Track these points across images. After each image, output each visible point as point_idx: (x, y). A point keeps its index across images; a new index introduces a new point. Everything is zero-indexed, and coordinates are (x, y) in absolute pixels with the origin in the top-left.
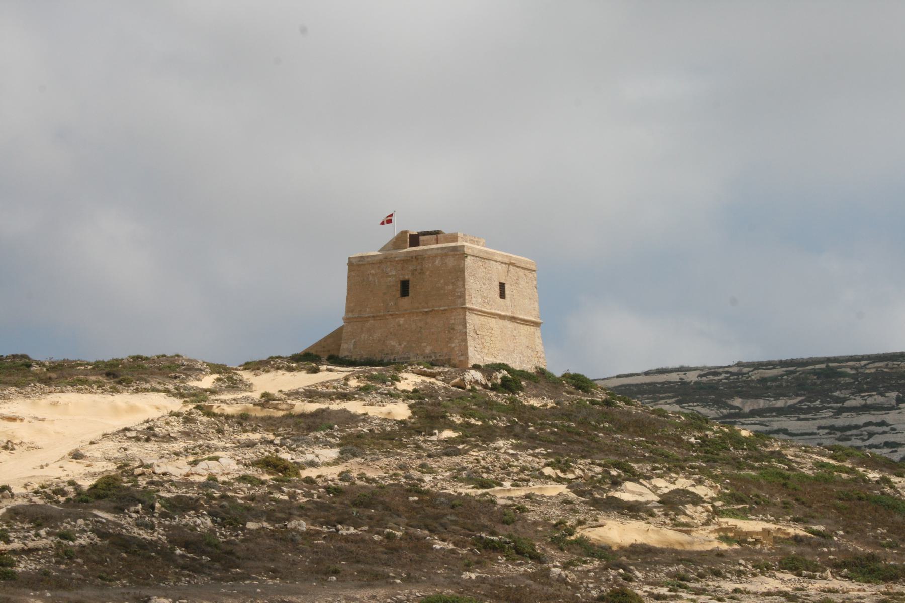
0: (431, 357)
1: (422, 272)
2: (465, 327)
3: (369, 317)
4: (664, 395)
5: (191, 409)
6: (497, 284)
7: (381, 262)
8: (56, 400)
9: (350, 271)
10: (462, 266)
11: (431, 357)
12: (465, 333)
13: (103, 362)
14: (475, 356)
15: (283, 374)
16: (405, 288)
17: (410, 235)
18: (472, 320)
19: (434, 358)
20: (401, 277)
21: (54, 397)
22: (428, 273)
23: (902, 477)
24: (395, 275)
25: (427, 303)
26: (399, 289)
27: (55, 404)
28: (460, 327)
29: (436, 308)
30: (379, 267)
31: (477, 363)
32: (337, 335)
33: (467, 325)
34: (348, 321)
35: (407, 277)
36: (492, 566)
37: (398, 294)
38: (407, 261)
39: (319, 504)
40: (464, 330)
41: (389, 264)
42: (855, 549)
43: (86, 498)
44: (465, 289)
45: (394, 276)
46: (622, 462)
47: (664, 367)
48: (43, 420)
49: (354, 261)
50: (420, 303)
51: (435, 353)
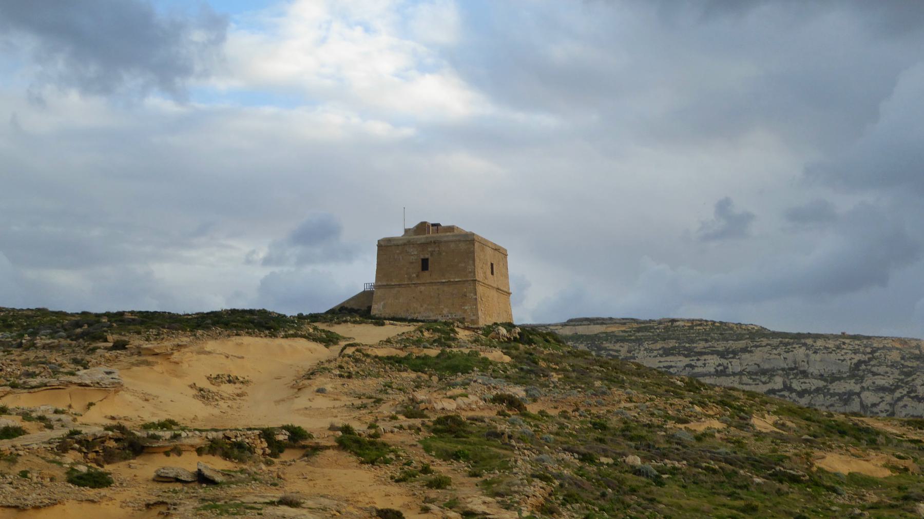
0: (448, 316)
1: (440, 253)
3: (395, 285)
5: (354, 352)
6: (489, 264)
7: (405, 244)
8: (240, 341)
9: (379, 250)
10: (472, 249)
11: (448, 316)
13: (832, 335)
16: (425, 265)
18: (480, 289)
20: (422, 257)
21: (236, 340)
22: (444, 254)
23: (922, 429)
27: (238, 344)
29: (452, 280)
32: (367, 296)
35: (427, 256)
36: (901, 464)
37: (420, 268)
40: (475, 297)
41: (412, 246)
43: (510, 413)
45: (415, 255)
47: (64, 311)
48: (243, 358)
49: (382, 243)
51: (451, 314)
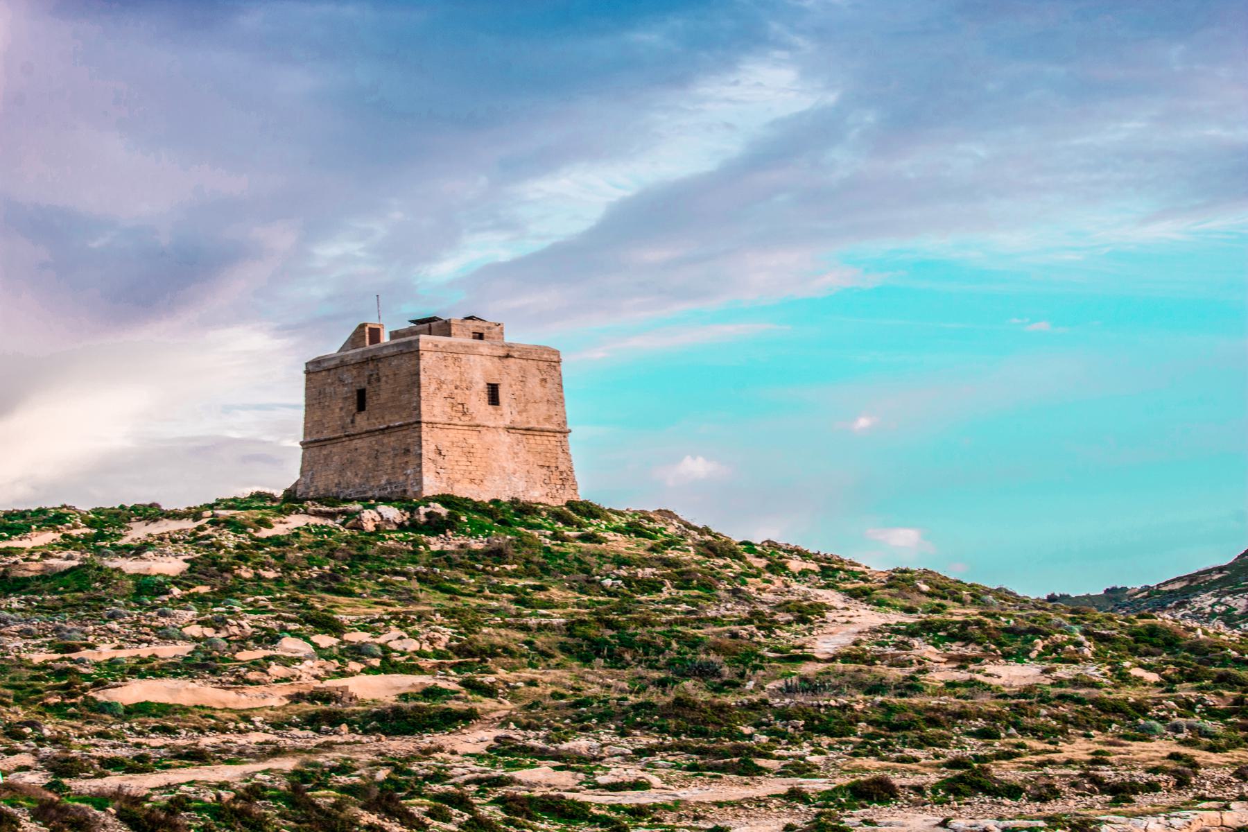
2: (420, 447)
4: (328, 509)
12: (421, 455)
14: (431, 485)
15: (167, 524)
17: (370, 329)
19: (389, 490)
23: (8, 787)
24: (352, 383)
25: (383, 418)
26: (356, 402)
28: (416, 448)
30: (335, 374)
31: (495, 497)
33: (424, 443)
34: (305, 446)
37: (354, 408)
38: (363, 362)
39: (397, 670)
40: (419, 452)
42: (749, 700)
44: (420, 397)
46: (154, 666)
50: (377, 419)
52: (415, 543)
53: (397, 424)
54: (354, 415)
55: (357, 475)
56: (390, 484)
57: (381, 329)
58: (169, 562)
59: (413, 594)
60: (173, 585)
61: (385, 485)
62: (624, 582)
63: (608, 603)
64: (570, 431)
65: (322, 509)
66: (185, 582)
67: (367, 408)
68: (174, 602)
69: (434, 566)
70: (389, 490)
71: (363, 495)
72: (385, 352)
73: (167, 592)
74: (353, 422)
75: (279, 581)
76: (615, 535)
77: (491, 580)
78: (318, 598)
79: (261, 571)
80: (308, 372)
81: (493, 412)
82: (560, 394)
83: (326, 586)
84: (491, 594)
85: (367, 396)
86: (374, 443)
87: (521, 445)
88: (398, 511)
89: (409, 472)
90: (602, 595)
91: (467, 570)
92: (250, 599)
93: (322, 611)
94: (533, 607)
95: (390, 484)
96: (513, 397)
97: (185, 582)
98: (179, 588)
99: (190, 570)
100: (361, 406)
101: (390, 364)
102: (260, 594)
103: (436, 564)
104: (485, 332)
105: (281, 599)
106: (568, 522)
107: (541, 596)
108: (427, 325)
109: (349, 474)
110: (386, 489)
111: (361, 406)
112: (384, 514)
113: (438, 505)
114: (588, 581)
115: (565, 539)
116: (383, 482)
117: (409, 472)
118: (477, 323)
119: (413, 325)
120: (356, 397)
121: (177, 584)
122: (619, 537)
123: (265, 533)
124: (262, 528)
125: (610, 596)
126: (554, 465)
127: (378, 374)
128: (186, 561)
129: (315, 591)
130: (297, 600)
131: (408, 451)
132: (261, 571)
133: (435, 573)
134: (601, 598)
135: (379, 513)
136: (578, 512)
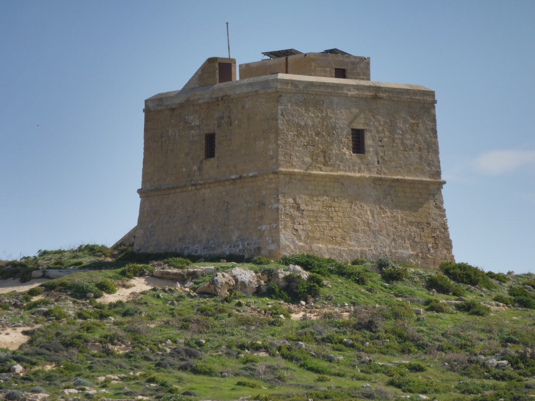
24: (199, 126)
26: (204, 147)
37: (202, 154)
40: (275, 206)
52: (275, 313)
53: (251, 174)
54: (202, 162)
55: (204, 229)
56: (243, 240)
57: (233, 64)
58: (7, 334)
59: (278, 374)
60: (15, 362)
61: (237, 241)
62: (510, 361)
63: (494, 388)
64: (444, 183)
65: (170, 270)
66: (28, 358)
67: (216, 154)
68: (19, 381)
69: (299, 340)
70: (241, 247)
71: (340, 353)
72: (238, 91)
73: (10, 370)
74: (200, 169)
75: (130, 357)
76: (498, 305)
77: (361, 357)
78: (176, 377)
79: (110, 346)
80: (147, 111)
81: (359, 161)
82: (433, 139)
83: (183, 363)
84: (363, 374)
85: (216, 141)
86: (224, 194)
87: (389, 198)
88: (254, 274)
89: (264, 228)
90: (487, 378)
91: (334, 345)
92: (102, 379)
93: (184, 394)
94: (410, 391)
95: (243, 240)
96: (380, 144)
97: (28, 358)
98: (22, 365)
99: (30, 342)
100: (210, 152)
101: (243, 107)
102: (112, 373)
103: (300, 338)
104: (348, 68)
105: (135, 378)
106: (443, 290)
107: (419, 377)
108: (284, 59)
109: (195, 227)
110: (238, 246)
111: (210, 152)
112: (239, 277)
113: (298, 268)
114: (470, 362)
115: (439, 309)
116: (234, 238)
117: (264, 228)
118: (340, 57)
119: (267, 57)
120: (204, 142)
121: (19, 360)
122: (503, 308)
123: (109, 299)
124: (105, 294)
125: (497, 379)
126: (425, 220)
127: (229, 117)
128: (25, 333)
129: (170, 369)
130: (151, 380)
131: (264, 204)
132: (110, 346)
133: (300, 347)
134: (486, 382)
135: (234, 277)
136: (453, 277)
